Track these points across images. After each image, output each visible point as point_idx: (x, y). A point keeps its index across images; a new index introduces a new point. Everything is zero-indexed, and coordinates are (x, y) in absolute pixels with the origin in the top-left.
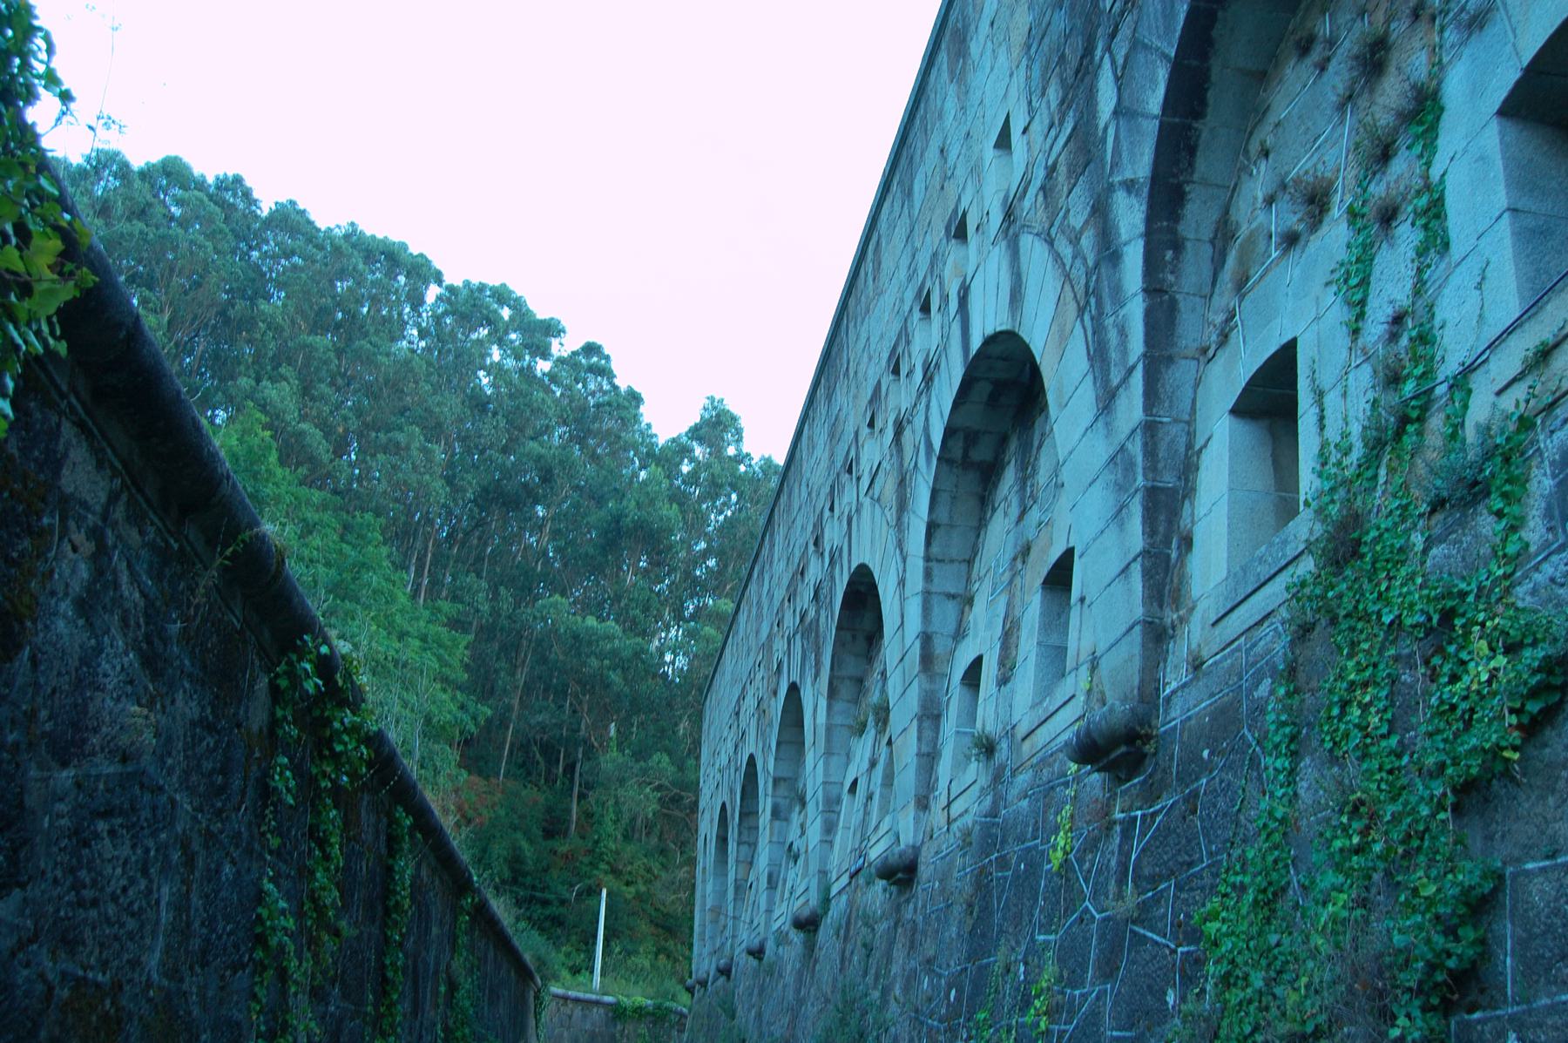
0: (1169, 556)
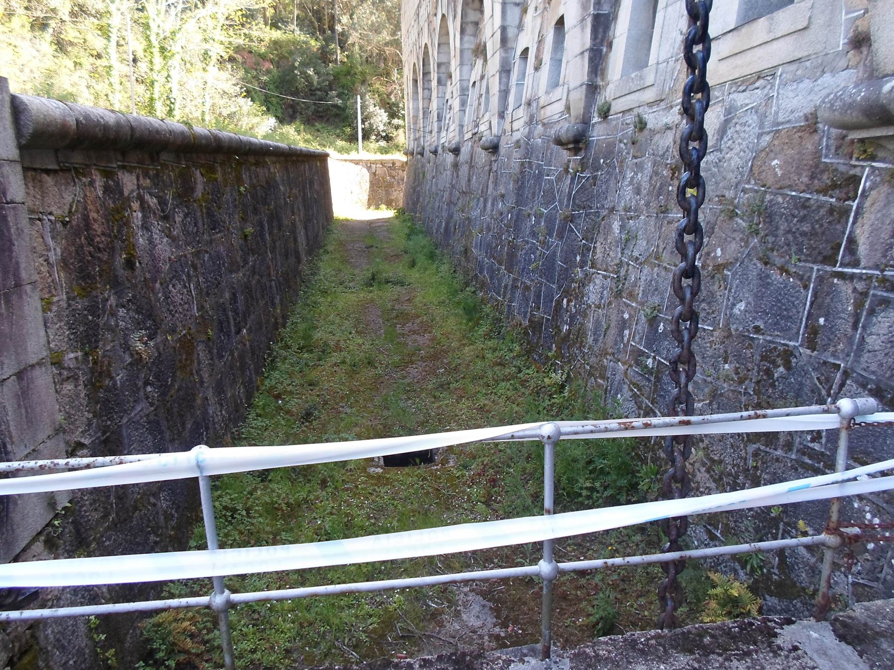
0: (602, 50)
